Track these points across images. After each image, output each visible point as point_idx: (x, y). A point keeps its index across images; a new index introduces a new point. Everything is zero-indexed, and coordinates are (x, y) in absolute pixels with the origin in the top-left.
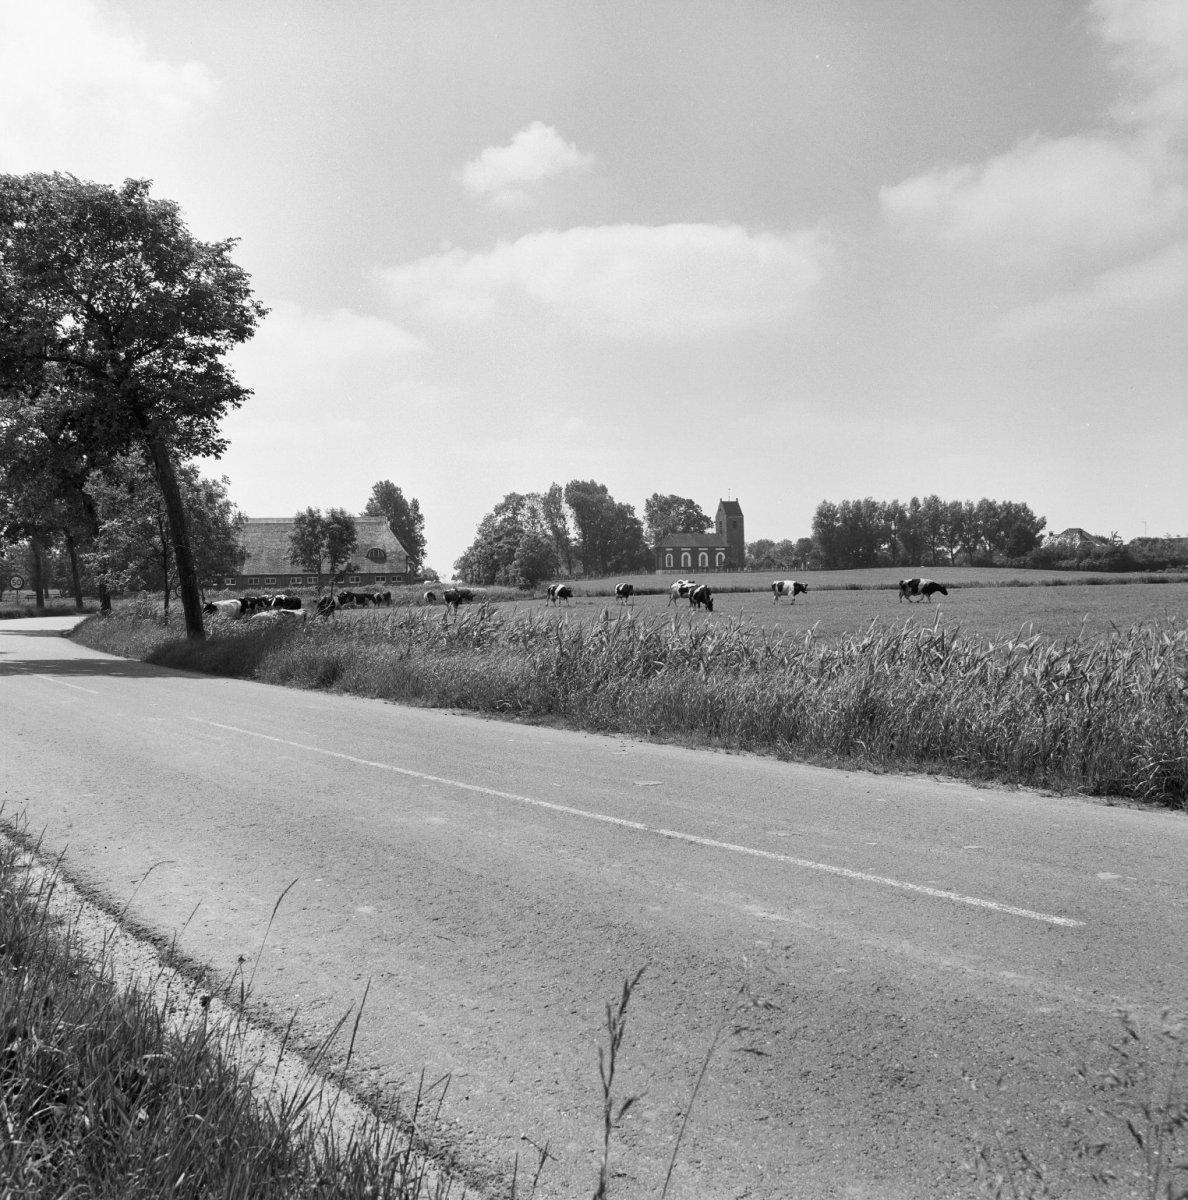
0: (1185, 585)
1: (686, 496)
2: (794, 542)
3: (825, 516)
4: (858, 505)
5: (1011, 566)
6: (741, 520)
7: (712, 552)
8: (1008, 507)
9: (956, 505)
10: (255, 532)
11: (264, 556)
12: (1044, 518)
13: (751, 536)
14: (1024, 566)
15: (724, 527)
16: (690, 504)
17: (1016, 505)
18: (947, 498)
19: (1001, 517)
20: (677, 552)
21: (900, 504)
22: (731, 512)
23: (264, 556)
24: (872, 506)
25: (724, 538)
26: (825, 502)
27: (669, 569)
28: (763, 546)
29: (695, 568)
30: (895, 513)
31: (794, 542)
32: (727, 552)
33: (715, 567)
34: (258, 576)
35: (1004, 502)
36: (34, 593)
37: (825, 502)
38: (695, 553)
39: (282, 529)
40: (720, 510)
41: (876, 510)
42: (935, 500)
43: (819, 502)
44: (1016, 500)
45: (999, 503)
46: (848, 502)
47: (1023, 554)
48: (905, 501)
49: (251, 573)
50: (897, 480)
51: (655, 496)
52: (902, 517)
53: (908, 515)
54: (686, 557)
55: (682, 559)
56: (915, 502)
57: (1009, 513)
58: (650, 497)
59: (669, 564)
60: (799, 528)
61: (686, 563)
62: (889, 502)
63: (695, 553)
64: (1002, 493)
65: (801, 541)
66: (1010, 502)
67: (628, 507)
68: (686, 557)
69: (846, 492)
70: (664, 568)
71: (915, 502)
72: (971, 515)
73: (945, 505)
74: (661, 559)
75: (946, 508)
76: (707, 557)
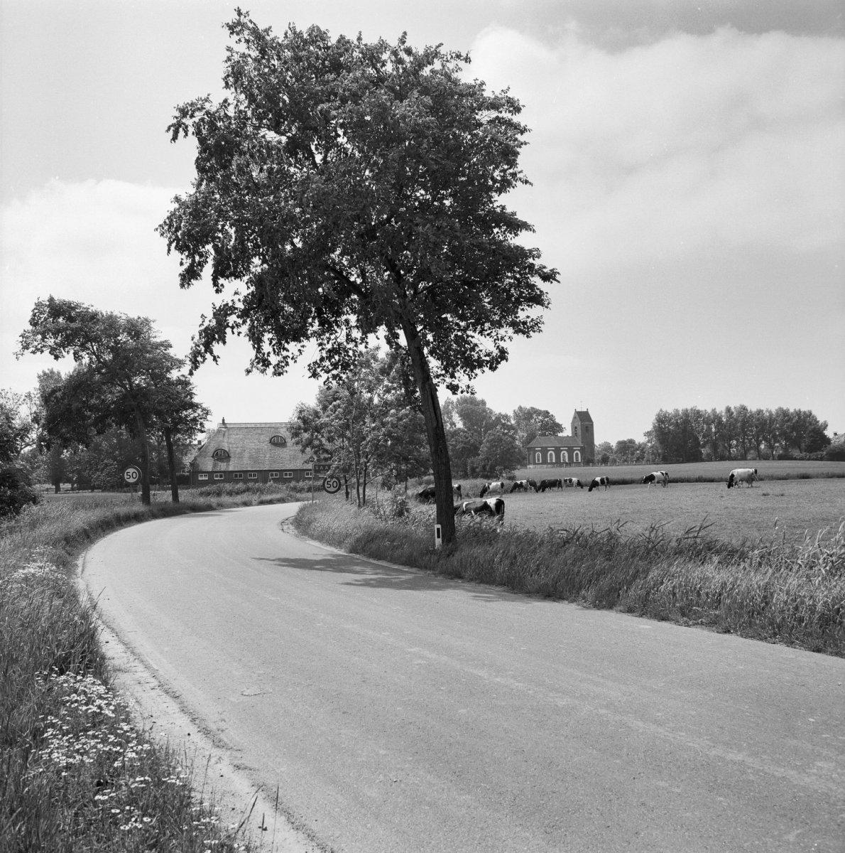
0: (818, 498)
1: (542, 408)
2: (614, 444)
3: (663, 422)
4: (686, 413)
5: (809, 460)
6: (592, 425)
7: (570, 450)
8: (798, 413)
9: (760, 412)
10: (237, 434)
11: (246, 455)
12: (825, 422)
13: (599, 440)
14: (821, 459)
15: (579, 432)
16: (546, 414)
17: (805, 412)
18: (752, 407)
19: (794, 421)
20: (544, 451)
21: (718, 411)
22: (584, 420)
23: (246, 455)
24: (698, 414)
25: (579, 440)
26: (661, 410)
27: (538, 464)
28: (607, 447)
29: (558, 463)
30: (716, 419)
31: (614, 444)
32: (582, 450)
33: (573, 462)
34: (243, 471)
35: (795, 410)
36: (54, 487)
37: (661, 410)
38: (558, 451)
39: (259, 431)
40: (575, 418)
41: (700, 416)
42: (744, 408)
43: (657, 411)
44: (804, 408)
45: (792, 410)
46: (687, 410)
47: (820, 449)
48: (721, 409)
49: (236, 469)
50: (712, 395)
51: (520, 408)
52: (720, 422)
53: (725, 420)
54: (551, 454)
55: (548, 455)
56: (728, 410)
57: (799, 418)
58: (516, 408)
59: (539, 460)
60: (639, 430)
61: (551, 459)
62: (709, 411)
63: (558, 451)
64: (793, 404)
65: (620, 443)
66: (800, 411)
67: (658, 415)
68: (577, 454)
69: (679, 401)
70: (535, 464)
71: (728, 410)
72: (772, 419)
73: (751, 412)
74: (531, 456)
75: (752, 416)
76: (579, 455)
